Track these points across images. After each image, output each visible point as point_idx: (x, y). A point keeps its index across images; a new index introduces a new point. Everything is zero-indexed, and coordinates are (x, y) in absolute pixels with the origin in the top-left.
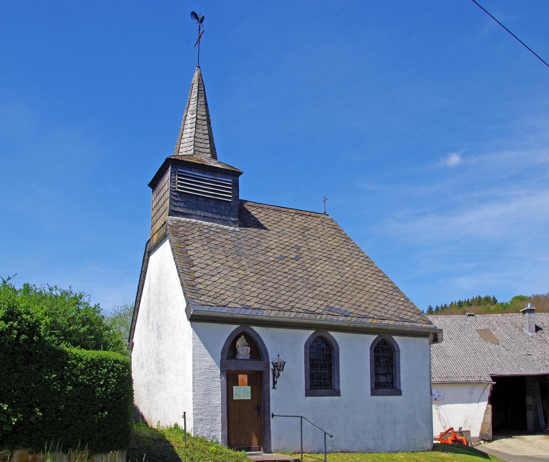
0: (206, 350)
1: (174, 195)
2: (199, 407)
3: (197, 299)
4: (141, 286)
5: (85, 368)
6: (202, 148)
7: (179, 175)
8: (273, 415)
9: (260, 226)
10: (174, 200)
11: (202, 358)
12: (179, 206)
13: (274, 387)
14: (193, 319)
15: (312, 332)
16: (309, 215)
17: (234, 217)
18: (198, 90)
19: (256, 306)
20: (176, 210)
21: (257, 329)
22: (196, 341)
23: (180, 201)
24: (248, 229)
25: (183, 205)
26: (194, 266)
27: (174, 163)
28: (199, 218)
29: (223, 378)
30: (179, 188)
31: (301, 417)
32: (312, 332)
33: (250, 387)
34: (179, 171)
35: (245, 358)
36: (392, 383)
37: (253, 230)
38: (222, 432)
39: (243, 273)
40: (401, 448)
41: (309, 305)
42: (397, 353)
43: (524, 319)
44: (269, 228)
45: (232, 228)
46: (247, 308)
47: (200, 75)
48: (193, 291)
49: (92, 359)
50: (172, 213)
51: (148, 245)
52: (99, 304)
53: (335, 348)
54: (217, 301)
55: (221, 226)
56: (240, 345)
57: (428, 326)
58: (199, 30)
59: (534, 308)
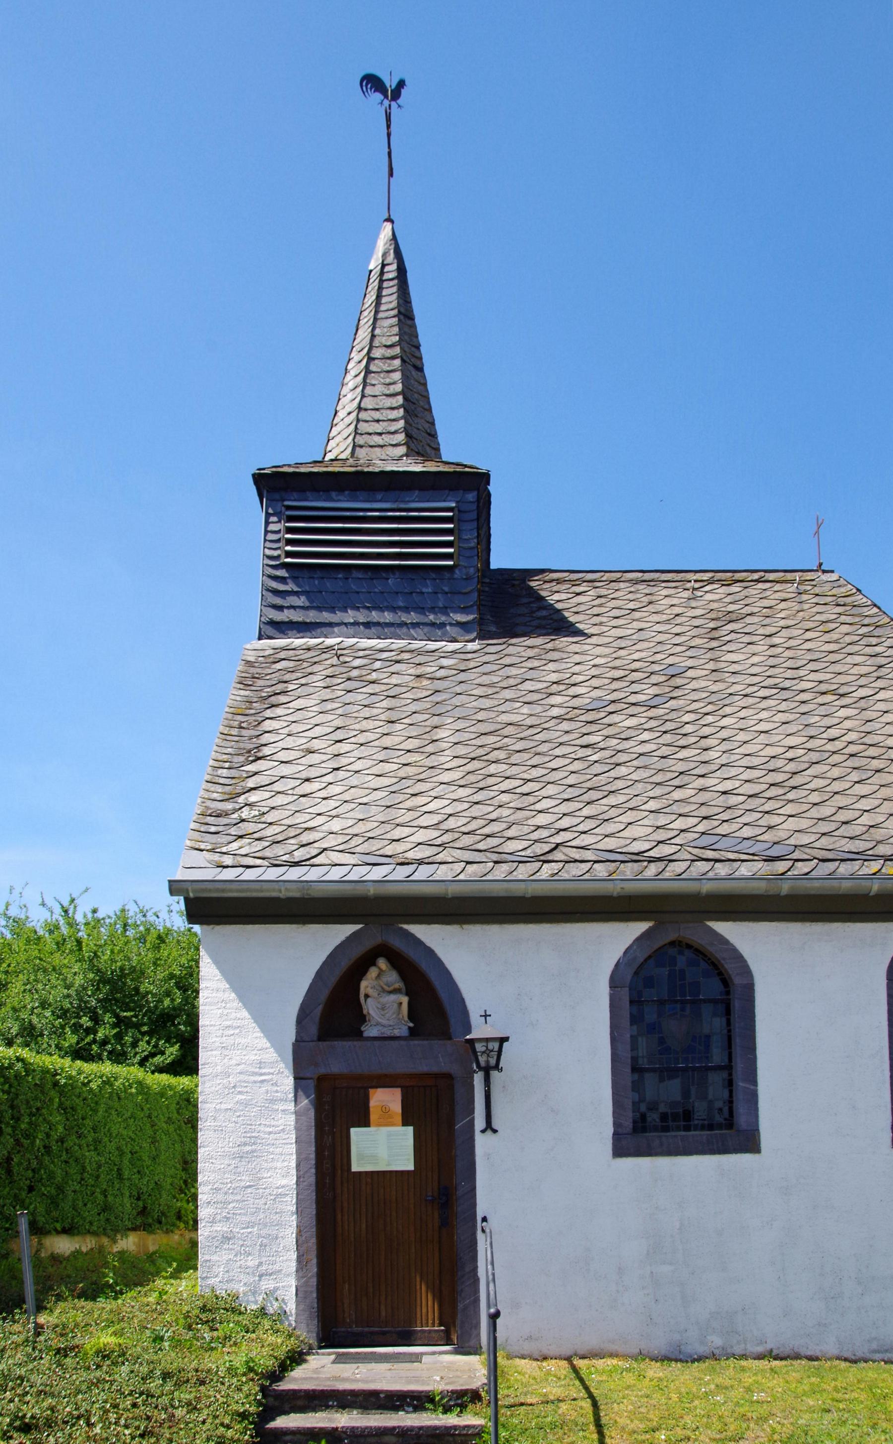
0: (245, 1013)
2: (220, 1197)
6: (380, 434)
7: (290, 519)
10: (276, 592)
11: (231, 1040)
15: (640, 928)
16: (758, 581)
17: (464, 610)
21: (429, 934)
25: (301, 601)
28: (351, 630)
29: (305, 1102)
30: (289, 554)
32: (640, 928)
33: (410, 1130)
34: (289, 508)
35: (388, 1032)
38: (298, 1279)
41: (637, 830)
52: (94, 911)
53: (737, 980)
56: (370, 991)
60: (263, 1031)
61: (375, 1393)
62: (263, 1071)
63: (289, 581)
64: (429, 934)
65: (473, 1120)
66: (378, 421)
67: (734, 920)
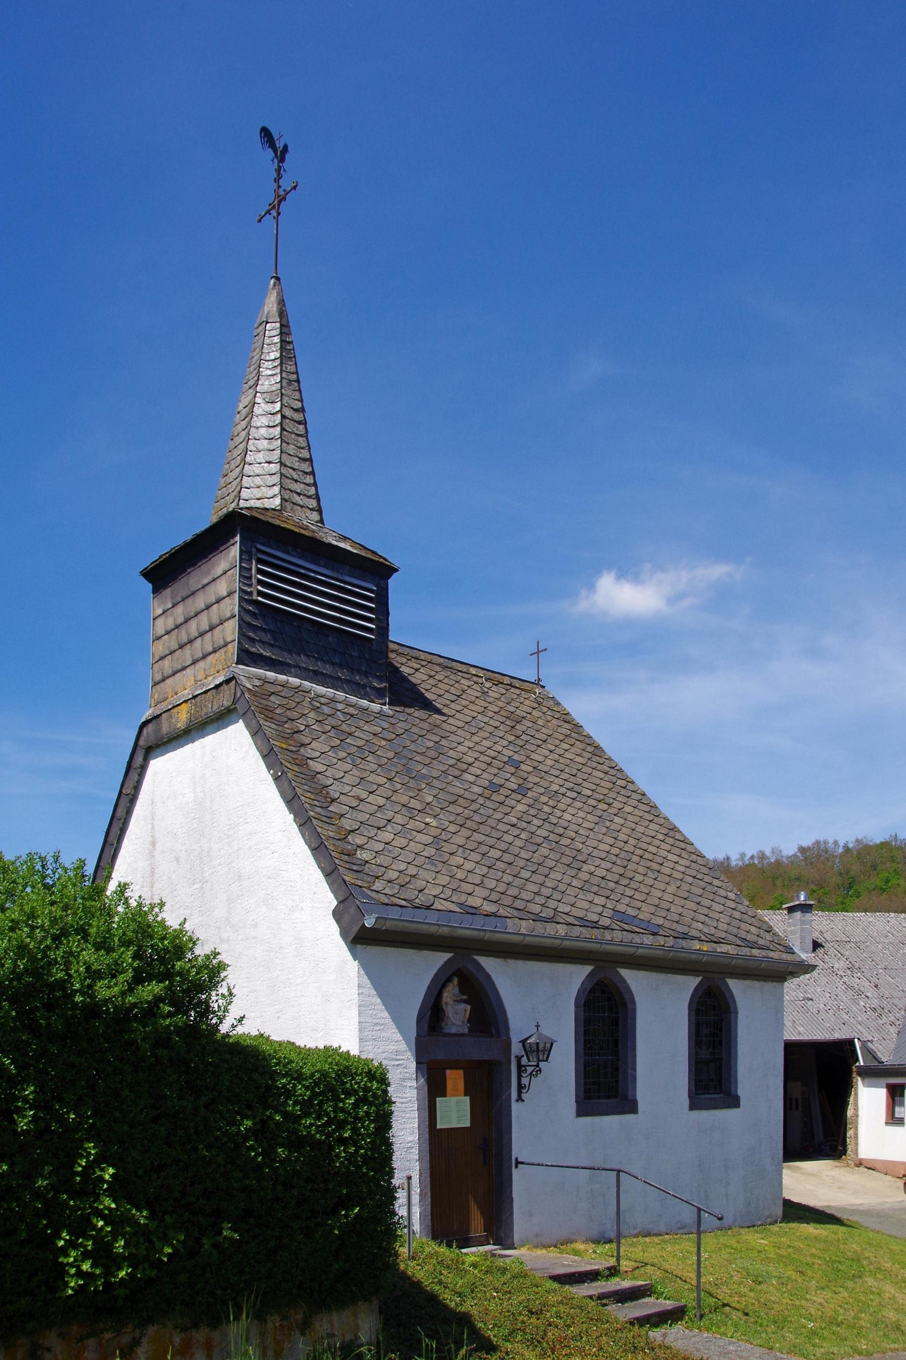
0: (386, 1014)
1: (248, 611)
3: (369, 888)
4: (115, 830)
5: (311, 1099)
6: (299, 494)
7: (260, 561)
8: (518, 1163)
9: (427, 705)
10: (249, 625)
12: (260, 641)
13: (520, 1099)
14: (360, 939)
17: (380, 679)
18: (282, 341)
19: (489, 908)
20: (253, 650)
21: (488, 963)
22: (364, 990)
23: (261, 629)
24: (408, 710)
25: (267, 638)
26: (333, 800)
27: (239, 525)
29: (422, 1080)
31: (619, 1171)
33: (468, 1098)
36: (720, 1080)
37: (417, 713)
39: (434, 824)
40: (735, 1221)
41: (578, 906)
42: (733, 1015)
43: (790, 925)
44: (445, 710)
45: (375, 707)
46: (473, 912)
47: (281, 302)
48: (355, 868)
49: (324, 1074)
50: (246, 657)
51: (145, 731)
54: (410, 894)
55: (353, 699)
57: (785, 956)
58: (277, 180)
59: (812, 902)
60: (398, 1028)
61: (572, 1275)
62: (398, 1057)
63: (259, 617)
64: (488, 963)
65: (510, 1093)
66: (296, 481)
67: (630, 968)
